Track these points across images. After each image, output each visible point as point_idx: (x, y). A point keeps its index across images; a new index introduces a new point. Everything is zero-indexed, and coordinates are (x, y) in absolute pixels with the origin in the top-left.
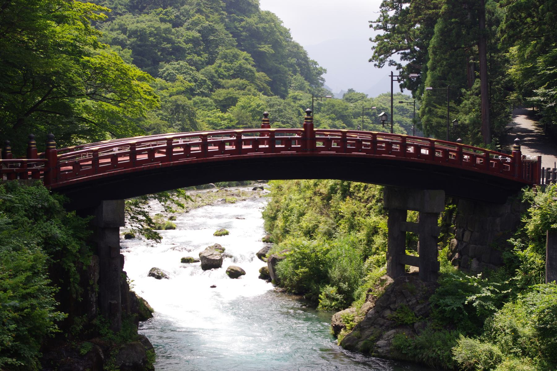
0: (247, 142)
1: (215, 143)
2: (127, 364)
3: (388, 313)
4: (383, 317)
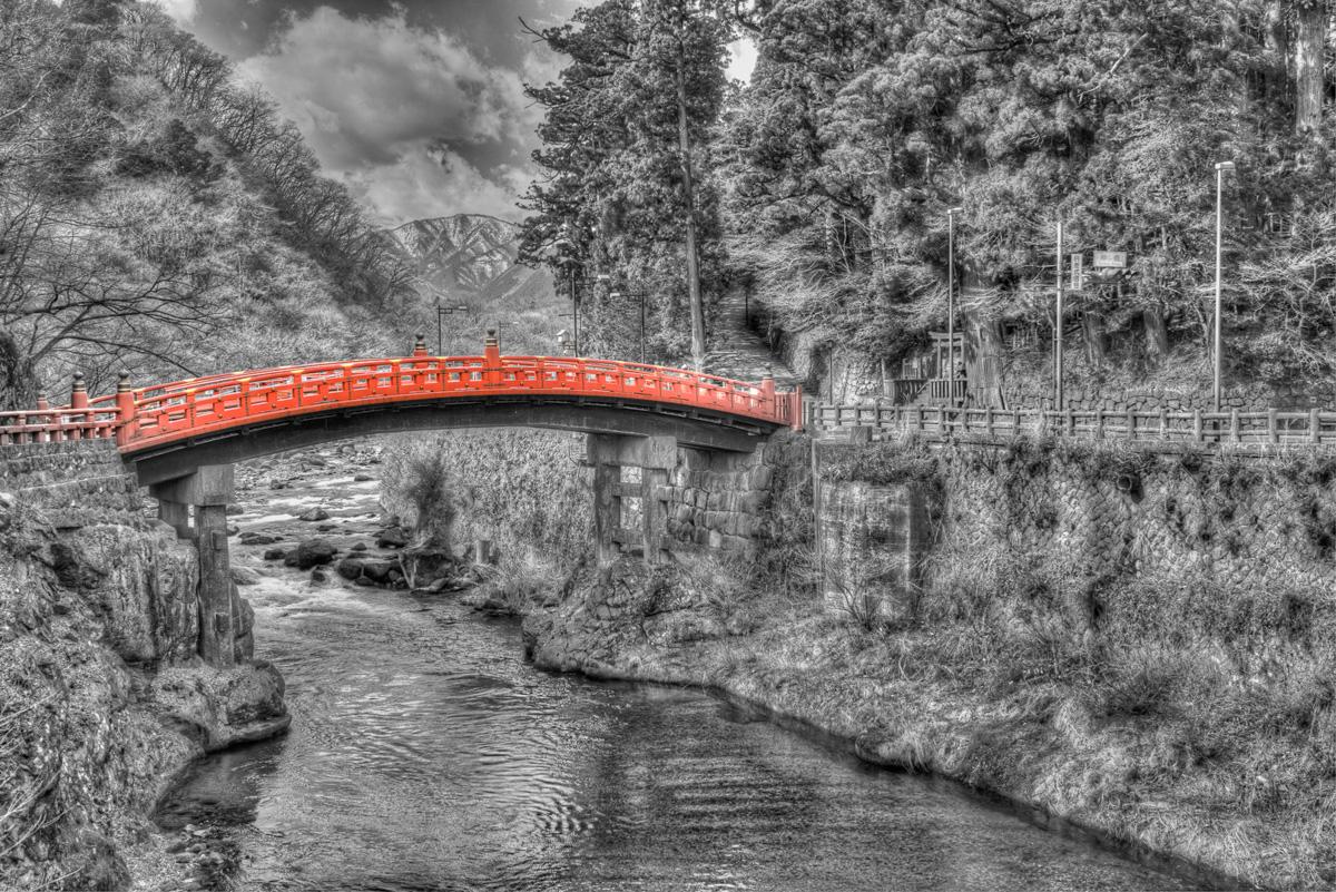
3: (604, 612)
4: (598, 618)
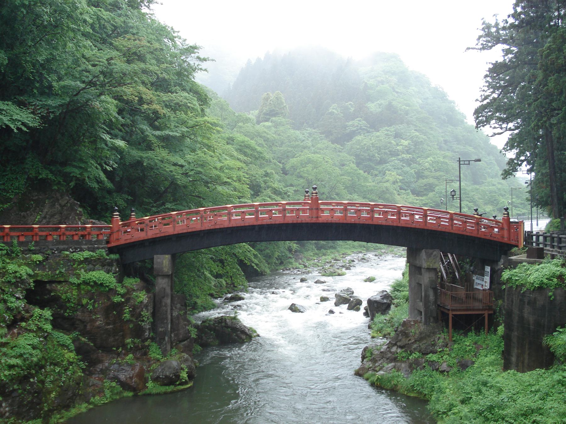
0: (292, 211)
1: (237, 214)
2: (161, 376)
3: (394, 349)
4: (391, 352)
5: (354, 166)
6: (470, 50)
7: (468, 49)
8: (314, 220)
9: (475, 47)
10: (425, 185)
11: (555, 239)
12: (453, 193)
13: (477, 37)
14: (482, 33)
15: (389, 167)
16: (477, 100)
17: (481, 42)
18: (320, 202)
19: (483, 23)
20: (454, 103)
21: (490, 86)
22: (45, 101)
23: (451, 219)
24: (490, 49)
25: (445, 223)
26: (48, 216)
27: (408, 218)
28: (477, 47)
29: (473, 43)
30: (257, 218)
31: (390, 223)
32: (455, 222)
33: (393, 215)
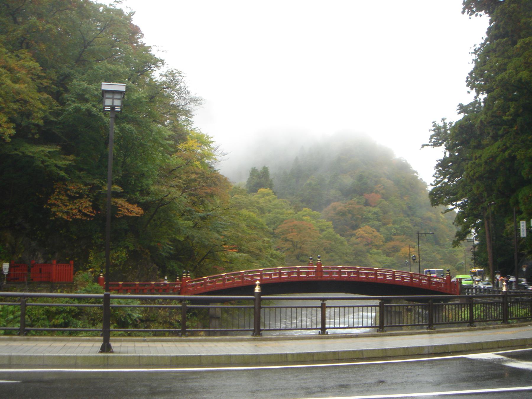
1: (266, 275)
5: (331, 230)
6: (425, 147)
7: (423, 146)
8: (319, 279)
9: (428, 143)
10: (393, 247)
11: (478, 290)
12: (414, 258)
13: (462, 10)
14: (433, 133)
15: (361, 232)
16: (469, 92)
17: (433, 140)
18: (322, 266)
19: (434, 126)
20: (417, 173)
21: (441, 173)
22: (481, 310)
23: (411, 278)
24: (439, 146)
25: (407, 280)
26: (140, 276)
27: (382, 277)
28: (430, 144)
29: (427, 142)
30: (299, 276)
31: (274, 281)
32: (414, 279)
33: (371, 275)
